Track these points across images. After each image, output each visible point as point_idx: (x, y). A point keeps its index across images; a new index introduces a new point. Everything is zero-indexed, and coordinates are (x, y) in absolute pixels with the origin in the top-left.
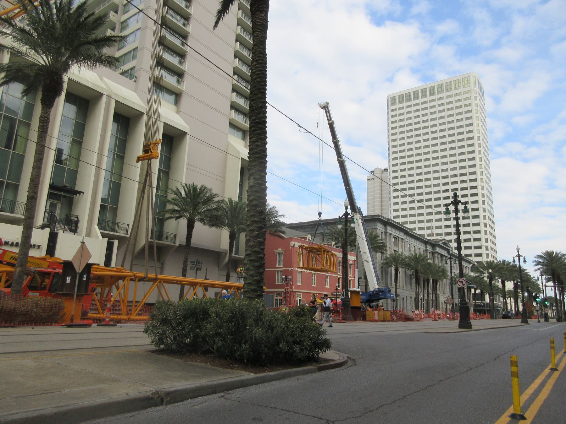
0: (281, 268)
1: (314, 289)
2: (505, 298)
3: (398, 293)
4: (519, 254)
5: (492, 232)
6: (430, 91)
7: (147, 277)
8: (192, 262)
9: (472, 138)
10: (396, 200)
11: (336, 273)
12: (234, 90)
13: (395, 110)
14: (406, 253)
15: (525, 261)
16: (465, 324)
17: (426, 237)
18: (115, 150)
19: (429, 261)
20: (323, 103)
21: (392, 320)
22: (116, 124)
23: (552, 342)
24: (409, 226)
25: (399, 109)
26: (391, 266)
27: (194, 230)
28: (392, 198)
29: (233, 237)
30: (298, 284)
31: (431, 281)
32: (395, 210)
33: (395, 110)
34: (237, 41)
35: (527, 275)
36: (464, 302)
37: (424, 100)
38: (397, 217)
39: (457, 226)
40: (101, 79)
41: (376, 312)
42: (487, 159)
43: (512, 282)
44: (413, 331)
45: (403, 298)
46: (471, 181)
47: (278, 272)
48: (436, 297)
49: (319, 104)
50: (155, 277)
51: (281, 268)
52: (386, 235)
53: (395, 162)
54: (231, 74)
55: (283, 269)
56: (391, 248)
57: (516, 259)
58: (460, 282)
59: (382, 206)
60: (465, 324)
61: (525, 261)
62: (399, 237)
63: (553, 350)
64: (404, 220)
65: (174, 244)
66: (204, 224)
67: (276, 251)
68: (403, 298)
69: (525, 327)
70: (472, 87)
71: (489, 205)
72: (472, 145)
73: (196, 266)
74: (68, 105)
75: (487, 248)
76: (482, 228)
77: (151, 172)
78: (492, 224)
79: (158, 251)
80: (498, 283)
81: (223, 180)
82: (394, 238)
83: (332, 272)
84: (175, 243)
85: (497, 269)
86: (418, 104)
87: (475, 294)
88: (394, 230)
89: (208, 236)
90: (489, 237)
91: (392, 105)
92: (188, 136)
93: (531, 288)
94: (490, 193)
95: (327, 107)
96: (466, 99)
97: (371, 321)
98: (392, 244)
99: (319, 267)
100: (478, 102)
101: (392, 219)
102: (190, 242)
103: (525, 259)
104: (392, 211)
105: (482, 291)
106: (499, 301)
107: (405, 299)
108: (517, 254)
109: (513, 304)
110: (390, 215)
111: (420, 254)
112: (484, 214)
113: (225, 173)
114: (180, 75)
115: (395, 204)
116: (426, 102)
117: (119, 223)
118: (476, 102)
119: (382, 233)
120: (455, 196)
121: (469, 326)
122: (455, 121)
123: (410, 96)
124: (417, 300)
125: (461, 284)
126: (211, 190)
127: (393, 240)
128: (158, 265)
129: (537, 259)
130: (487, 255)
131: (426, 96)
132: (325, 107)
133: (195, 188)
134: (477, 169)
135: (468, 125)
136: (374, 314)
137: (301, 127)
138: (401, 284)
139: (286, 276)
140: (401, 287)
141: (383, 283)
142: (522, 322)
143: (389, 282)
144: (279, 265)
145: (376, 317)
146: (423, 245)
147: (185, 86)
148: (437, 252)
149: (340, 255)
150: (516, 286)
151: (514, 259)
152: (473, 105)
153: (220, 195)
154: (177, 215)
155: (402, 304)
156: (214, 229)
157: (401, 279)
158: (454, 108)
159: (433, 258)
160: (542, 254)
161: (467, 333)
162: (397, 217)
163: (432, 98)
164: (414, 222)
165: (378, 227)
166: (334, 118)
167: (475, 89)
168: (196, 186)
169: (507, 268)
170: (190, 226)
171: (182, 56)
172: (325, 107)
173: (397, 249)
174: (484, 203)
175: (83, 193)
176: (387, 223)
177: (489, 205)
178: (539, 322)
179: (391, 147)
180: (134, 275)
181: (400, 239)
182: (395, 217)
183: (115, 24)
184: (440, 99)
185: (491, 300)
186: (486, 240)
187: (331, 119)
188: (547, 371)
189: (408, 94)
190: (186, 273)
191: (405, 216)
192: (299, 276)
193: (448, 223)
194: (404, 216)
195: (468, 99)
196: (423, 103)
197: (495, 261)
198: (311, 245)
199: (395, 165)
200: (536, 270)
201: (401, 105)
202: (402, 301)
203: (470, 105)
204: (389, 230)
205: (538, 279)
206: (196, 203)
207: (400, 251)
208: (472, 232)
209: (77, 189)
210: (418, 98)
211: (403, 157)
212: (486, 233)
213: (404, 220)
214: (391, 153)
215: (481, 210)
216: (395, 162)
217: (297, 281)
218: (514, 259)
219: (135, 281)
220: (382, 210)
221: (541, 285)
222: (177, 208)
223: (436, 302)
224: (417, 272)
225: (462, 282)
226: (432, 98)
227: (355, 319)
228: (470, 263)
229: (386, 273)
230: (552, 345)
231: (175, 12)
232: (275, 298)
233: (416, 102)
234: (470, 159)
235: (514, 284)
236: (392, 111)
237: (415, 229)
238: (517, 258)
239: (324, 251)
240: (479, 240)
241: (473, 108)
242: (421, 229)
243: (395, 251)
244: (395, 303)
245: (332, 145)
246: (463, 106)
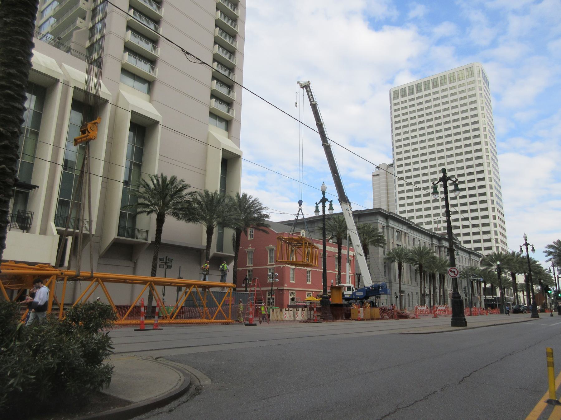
0: (273, 265)
1: (309, 286)
2: (516, 290)
3: (402, 290)
4: (526, 243)
5: (502, 224)
6: (433, 83)
7: (78, 276)
8: (160, 260)
9: (477, 129)
10: (402, 195)
11: (317, 268)
12: (129, 27)
13: (398, 104)
14: (410, 247)
15: (533, 250)
16: (458, 320)
17: (433, 231)
18: (132, 159)
19: (435, 254)
20: (304, 81)
21: (383, 318)
22: (132, 133)
23: (550, 354)
24: (416, 221)
25: (402, 102)
26: (394, 261)
27: (164, 225)
28: (397, 193)
29: (210, 232)
30: (291, 282)
31: (437, 276)
32: (401, 205)
33: (398, 104)
34: (216, 26)
35: (539, 267)
36: (456, 295)
37: (427, 92)
38: (404, 212)
39: (447, 206)
40: (61, 66)
41: (362, 309)
42: (494, 150)
43: (523, 274)
44: (385, 332)
45: (408, 295)
46: (479, 172)
47: (270, 269)
48: (444, 293)
49: (298, 83)
50: (89, 275)
51: (273, 265)
52: (388, 230)
53: (400, 156)
54: (126, 8)
55: (275, 266)
56: (393, 242)
57: (524, 248)
58: (451, 272)
59: (388, 202)
60: (458, 320)
61: (533, 250)
62: (402, 231)
63: (551, 369)
64: (411, 215)
65: (146, 242)
66: (179, 219)
67: (267, 248)
68: (408, 295)
69: (536, 322)
70: (476, 77)
71: (498, 197)
72: (478, 136)
73: (166, 263)
74: (74, 112)
75: (497, 241)
76: (491, 220)
77: (89, 157)
78: (501, 216)
79: (124, 250)
80: (507, 275)
81: (204, 173)
82: (397, 232)
83: (315, 267)
84: (147, 240)
85: (505, 260)
86: (421, 97)
87: (485, 288)
88: (396, 224)
89: (177, 229)
90: (498, 229)
91: (395, 98)
92: (160, 127)
93: (544, 281)
94: (498, 185)
95: (309, 87)
96: (470, 90)
97: (357, 320)
98: (395, 238)
99: (300, 260)
100: (483, 92)
101: (398, 214)
102: (160, 238)
103: (533, 248)
104: (398, 206)
105: (492, 285)
106: (509, 295)
107: (411, 295)
108: (524, 242)
109: (526, 297)
110: (397, 210)
111: (424, 248)
112: (493, 206)
113: (206, 165)
114: (152, 61)
115: (401, 199)
116: (429, 95)
117: (138, 229)
118: (481, 92)
119: (383, 227)
120: (444, 171)
121: (464, 324)
122: (460, 113)
123: (413, 89)
124: (423, 296)
125: (452, 274)
126: (182, 181)
127: (396, 234)
128: (132, 264)
129: (548, 250)
130: (498, 248)
131: (429, 88)
132: (306, 87)
133: (164, 179)
134: (484, 161)
135: (473, 116)
136: (359, 312)
137: (188, 53)
138: (406, 280)
139: (272, 273)
140: (406, 283)
141: (386, 279)
142: (532, 317)
143: (392, 277)
144: (270, 262)
145: (362, 316)
146: (428, 238)
147: (158, 73)
148: (443, 246)
149: (321, 247)
150: (528, 279)
151: (521, 249)
152: (478, 95)
153: (191, 185)
154: (149, 210)
155: (407, 300)
156: (191, 224)
157: (405, 274)
158: (458, 99)
159: (440, 252)
160: (553, 244)
161: (461, 332)
162: (404, 212)
163: (436, 90)
164: (421, 217)
165: (379, 221)
166: (317, 99)
167: (479, 79)
168: (166, 178)
169: (517, 260)
170: (160, 221)
171: (154, 42)
172: (306, 87)
173: (400, 244)
174: (492, 195)
175: (38, 187)
176: (388, 216)
177: (498, 197)
178: (552, 315)
179: (395, 142)
180: (62, 274)
181: (403, 233)
182: (402, 212)
183: (85, 12)
184: (443, 91)
185: (502, 294)
186: (496, 233)
187: (314, 101)
188: (541, 405)
189: (411, 88)
190: (155, 271)
191: (411, 211)
192: (292, 274)
193: (436, 204)
194: (410, 211)
195: (473, 89)
196: (426, 96)
197: (504, 253)
198: (290, 236)
199: (400, 159)
200: (547, 261)
201: (404, 99)
202: (407, 297)
203: (474, 95)
204: (391, 223)
205: (550, 270)
206: (167, 196)
207: (404, 245)
208: (470, 219)
209: (33, 183)
210: (421, 91)
211: (408, 151)
212: (495, 225)
213: (411, 215)
214: (395, 148)
215: (489, 202)
216: (400, 156)
217: (289, 278)
218: (521, 249)
219: (63, 279)
220: (388, 206)
221: (553, 276)
222: (147, 202)
223: (444, 297)
224: (421, 266)
225: (454, 272)
226: (436, 90)
227: (336, 317)
228: (479, 256)
229: (390, 269)
230: (550, 359)
231: (223, 48)
232: (267, 297)
233: (419, 94)
234: (476, 151)
235: (526, 276)
236: (395, 105)
237: (422, 224)
238: (525, 247)
239: (306, 243)
240: (488, 232)
241: (478, 98)
242: (428, 223)
243: (398, 245)
244: (398, 299)
245: (316, 128)
246: (467, 97)
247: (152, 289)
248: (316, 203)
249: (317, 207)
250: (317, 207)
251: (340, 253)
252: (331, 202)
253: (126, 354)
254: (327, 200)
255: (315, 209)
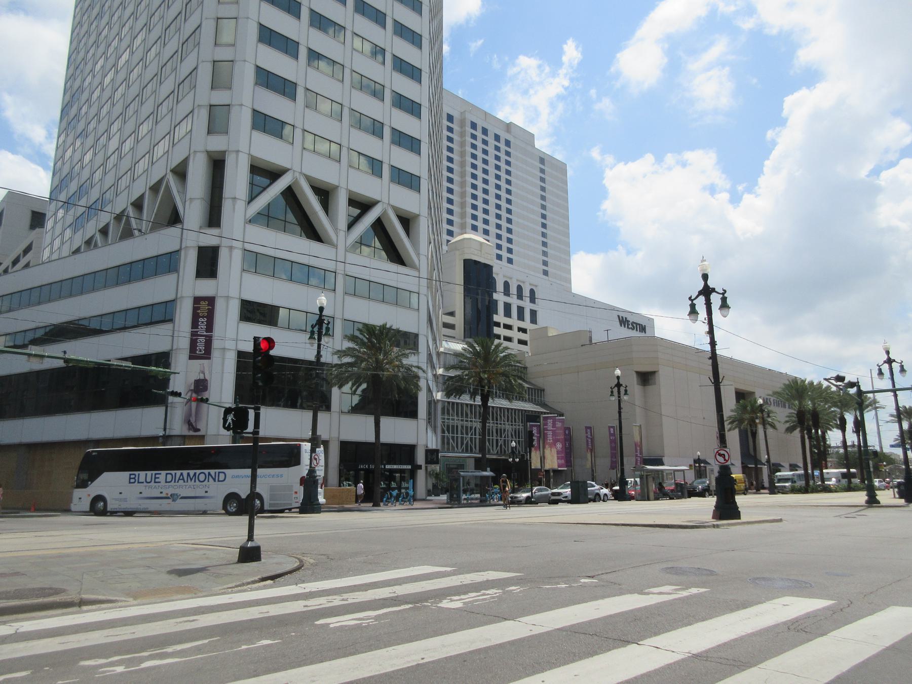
15: (902, 370)
16: (727, 510)
50: (260, 471)
60: (727, 510)
108: (885, 357)
238: (886, 366)
247: (896, 396)
248: (690, 298)
249: (693, 306)
250: (693, 306)
251: (484, 427)
252: (723, 294)
253: (218, 563)
254: (713, 290)
255: (689, 309)
